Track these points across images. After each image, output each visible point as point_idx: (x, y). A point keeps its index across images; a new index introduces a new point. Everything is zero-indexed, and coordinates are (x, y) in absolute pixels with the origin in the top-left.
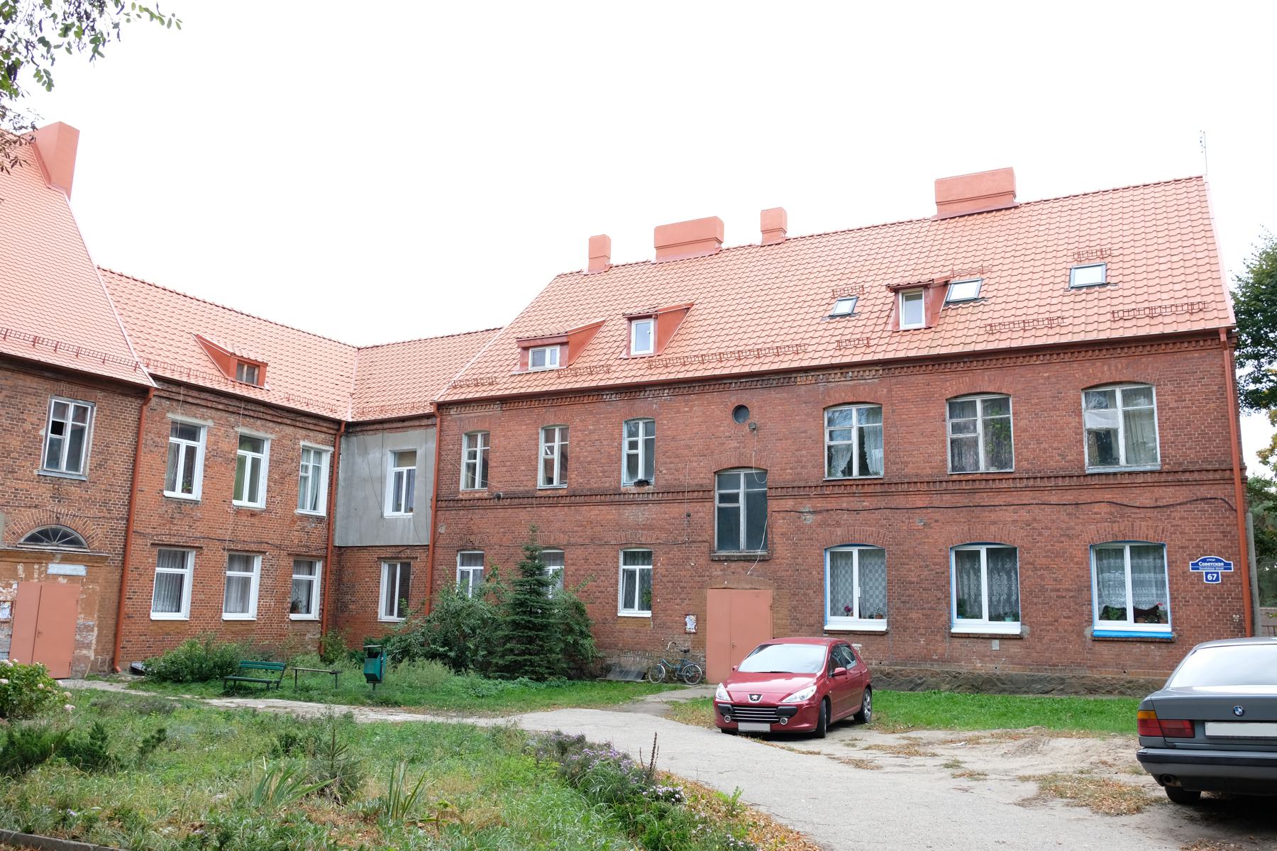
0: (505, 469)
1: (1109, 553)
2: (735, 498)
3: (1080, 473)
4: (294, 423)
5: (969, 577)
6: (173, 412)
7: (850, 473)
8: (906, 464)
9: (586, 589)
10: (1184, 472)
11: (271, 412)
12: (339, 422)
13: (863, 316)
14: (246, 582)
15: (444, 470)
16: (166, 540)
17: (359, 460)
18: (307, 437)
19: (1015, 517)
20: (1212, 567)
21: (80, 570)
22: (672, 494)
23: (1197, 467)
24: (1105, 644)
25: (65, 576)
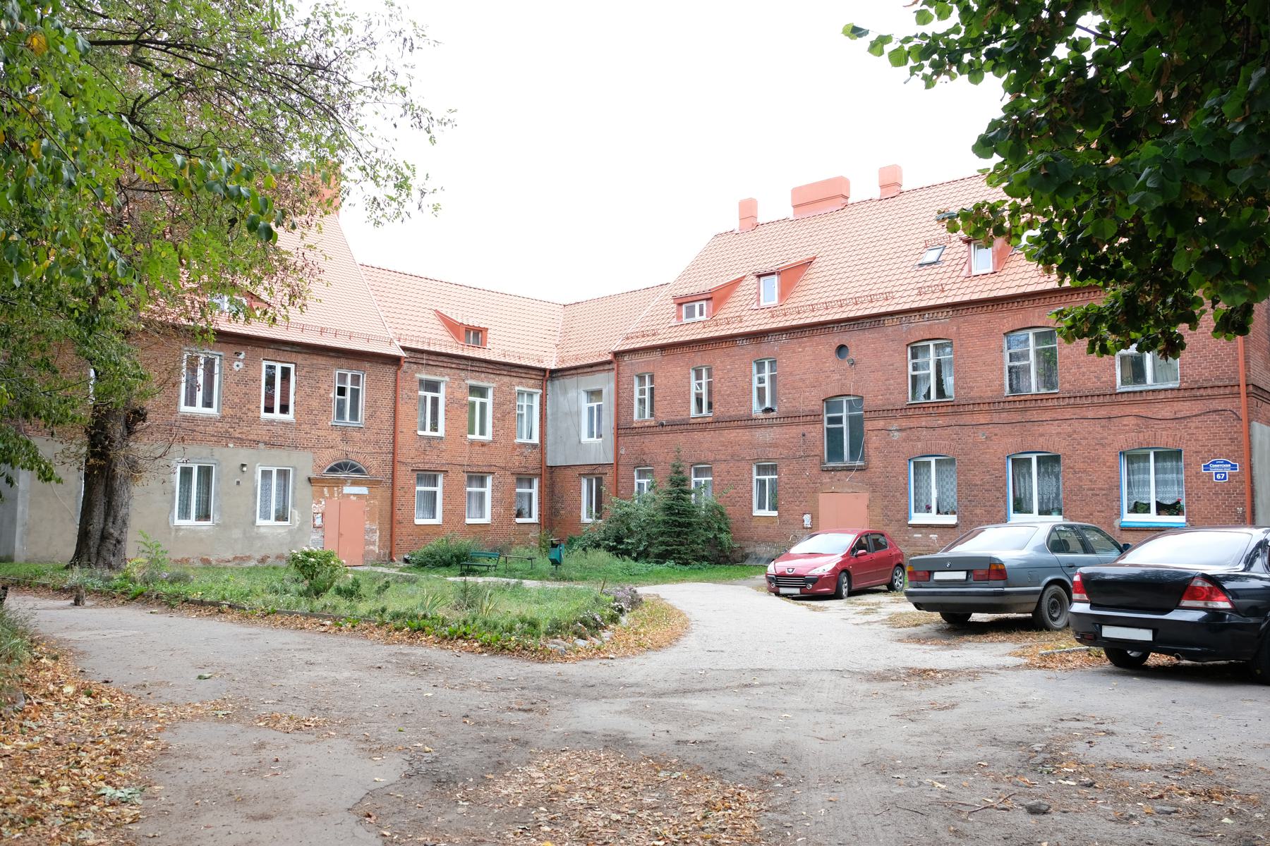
0: (666, 402)
1: (1135, 458)
2: (839, 420)
3: (1112, 392)
4: (509, 373)
5: (1025, 479)
6: (419, 373)
7: (929, 398)
8: (972, 388)
9: (729, 495)
10: (1199, 388)
11: (492, 367)
12: (544, 370)
13: (947, 263)
14: (482, 495)
15: (622, 406)
16: (421, 466)
17: (561, 399)
18: (521, 384)
19: (1059, 430)
20: (1220, 468)
21: (363, 490)
22: (791, 418)
23: (1210, 384)
24: (1131, 533)
25: (354, 495)
